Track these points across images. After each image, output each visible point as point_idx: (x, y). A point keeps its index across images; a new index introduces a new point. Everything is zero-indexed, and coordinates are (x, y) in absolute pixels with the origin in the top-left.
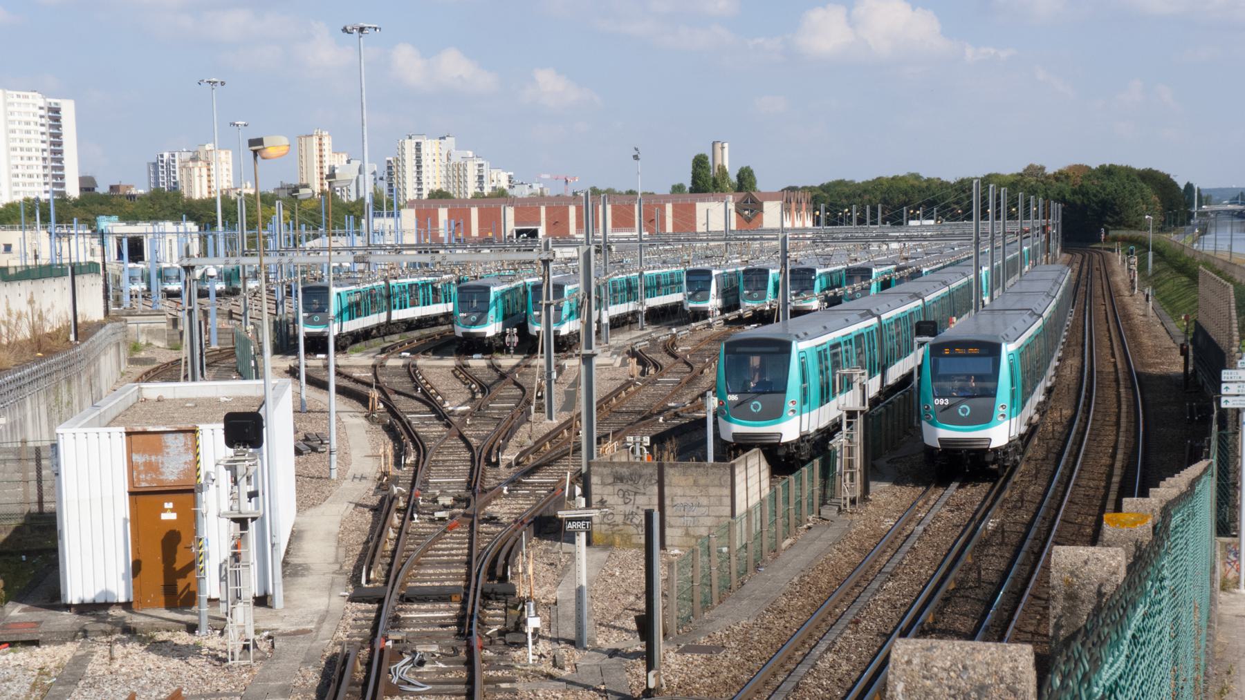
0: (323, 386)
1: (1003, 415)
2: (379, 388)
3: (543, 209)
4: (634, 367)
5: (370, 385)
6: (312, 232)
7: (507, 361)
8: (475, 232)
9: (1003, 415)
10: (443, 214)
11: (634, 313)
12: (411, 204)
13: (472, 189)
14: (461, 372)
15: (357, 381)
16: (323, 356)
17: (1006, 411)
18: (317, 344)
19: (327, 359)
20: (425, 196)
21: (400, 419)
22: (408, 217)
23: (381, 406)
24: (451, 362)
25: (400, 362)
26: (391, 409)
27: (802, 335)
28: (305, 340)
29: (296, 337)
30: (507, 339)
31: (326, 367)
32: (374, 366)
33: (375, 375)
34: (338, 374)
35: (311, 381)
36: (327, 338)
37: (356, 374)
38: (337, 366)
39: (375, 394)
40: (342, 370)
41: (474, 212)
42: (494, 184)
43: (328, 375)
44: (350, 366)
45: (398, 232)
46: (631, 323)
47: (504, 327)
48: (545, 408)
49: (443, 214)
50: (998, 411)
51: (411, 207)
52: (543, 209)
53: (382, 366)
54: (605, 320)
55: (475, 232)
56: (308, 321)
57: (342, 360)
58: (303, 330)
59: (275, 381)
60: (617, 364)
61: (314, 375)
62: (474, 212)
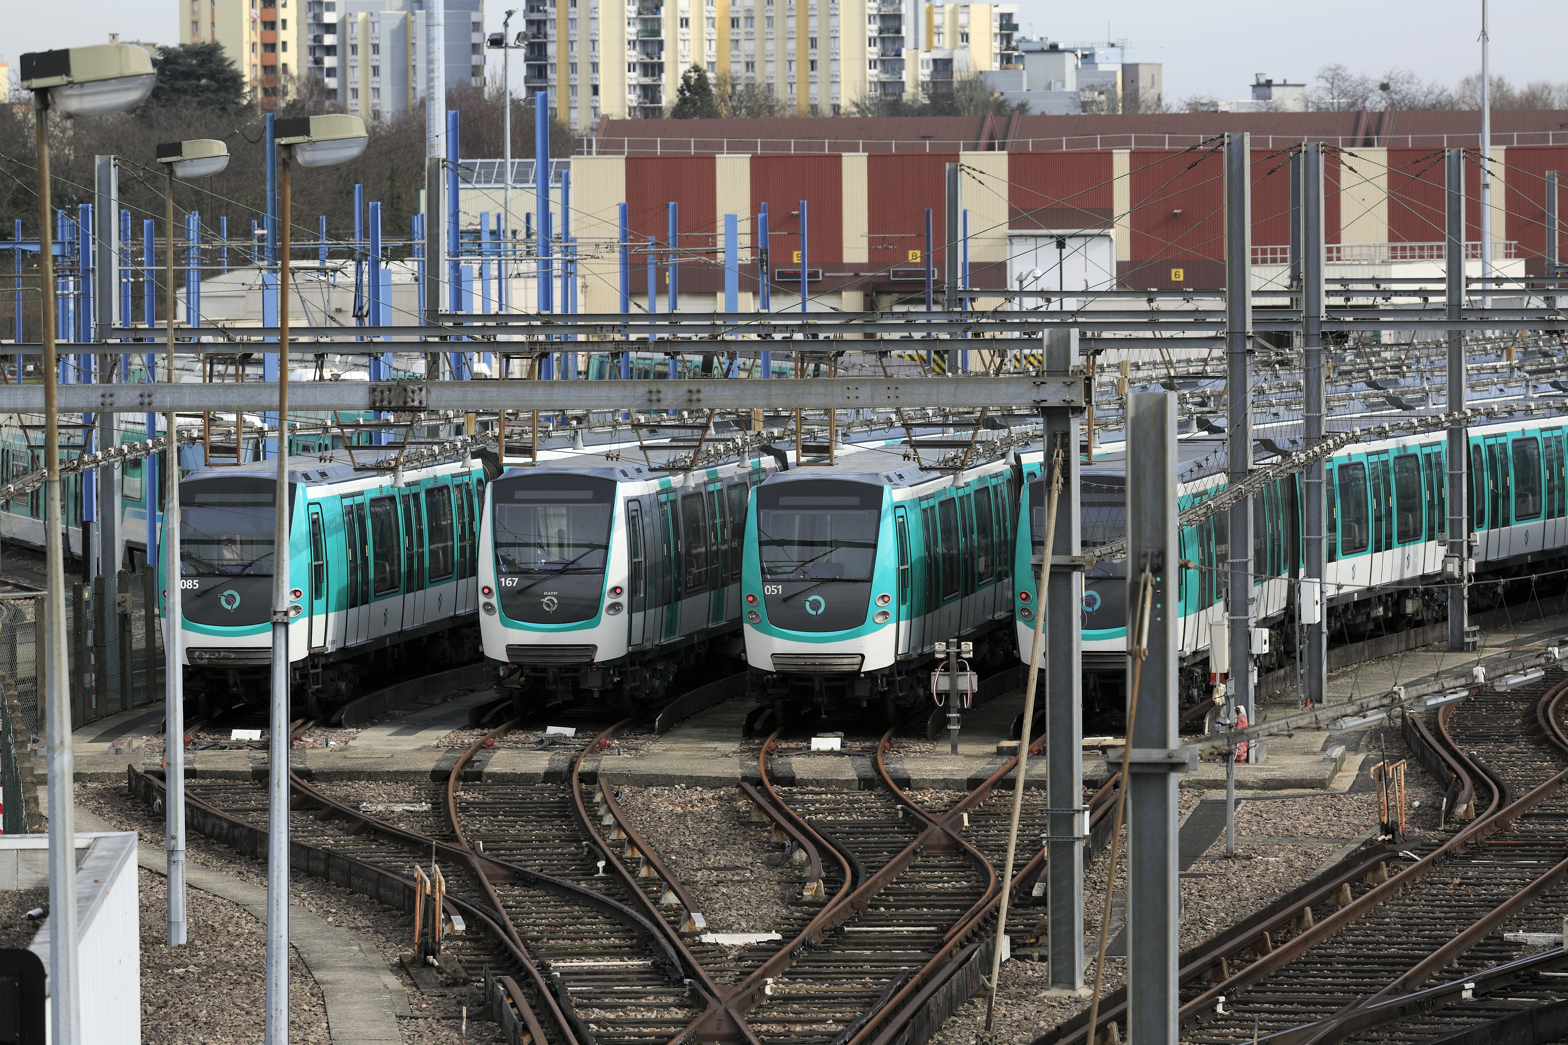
0: (242, 846)
1: (885, 614)
2: (455, 862)
3: (1121, 161)
4: (1405, 794)
5: (415, 847)
6: (223, 242)
7: (935, 765)
8: (855, 247)
9: (885, 614)
10: (733, 180)
11: (1431, 587)
12: (610, 135)
13: (851, 81)
14: (763, 813)
15: (373, 830)
16: (255, 735)
17: (891, 607)
18: (227, 694)
19: (266, 745)
20: (669, 97)
21: (524, 978)
22: (597, 189)
23: (459, 925)
24: (721, 758)
25: (539, 763)
26: (493, 947)
27: (315, 477)
28: (189, 673)
29: (156, 659)
30: (940, 682)
31: (262, 777)
32: (440, 776)
33: (440, 807)
34: (300, 802)
35: (208, 833)
36: (265, 673)
37: (376, 803)
38: (299, 775)
39: (432, 880)
40: (322, 790)
41: (855, 170)
42: (943, 48)
43: (266, 809)
44: (353, 775)
45: (549, 244)
46: (1416, 623)
47: (923, 636)
48: (1041, 928)
49: (733, 180)
50: (875, 606)
51: (607, 148)
52: (1121, 161)
53: (471, 776)
54: (1312, 613)
55: (855, 247)
56: (199, 609)
57: (328, 748)
58: (181, 639)
59: (81, 841)
60: (1344, 782)
61: (217, 806)
62: (855, 170)
